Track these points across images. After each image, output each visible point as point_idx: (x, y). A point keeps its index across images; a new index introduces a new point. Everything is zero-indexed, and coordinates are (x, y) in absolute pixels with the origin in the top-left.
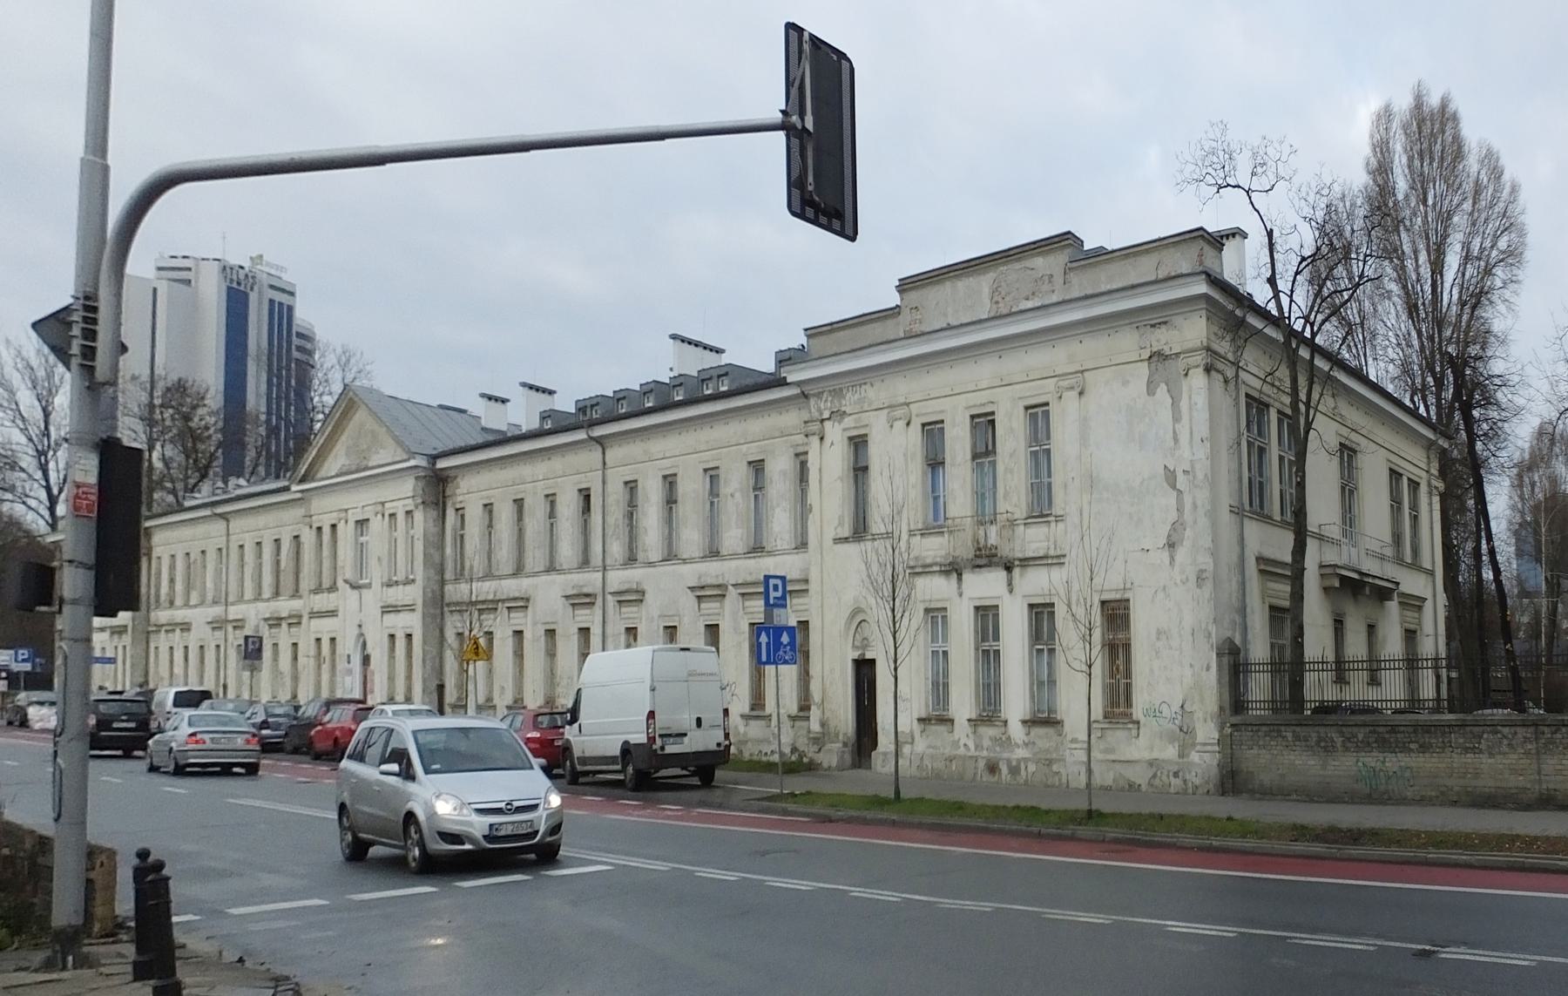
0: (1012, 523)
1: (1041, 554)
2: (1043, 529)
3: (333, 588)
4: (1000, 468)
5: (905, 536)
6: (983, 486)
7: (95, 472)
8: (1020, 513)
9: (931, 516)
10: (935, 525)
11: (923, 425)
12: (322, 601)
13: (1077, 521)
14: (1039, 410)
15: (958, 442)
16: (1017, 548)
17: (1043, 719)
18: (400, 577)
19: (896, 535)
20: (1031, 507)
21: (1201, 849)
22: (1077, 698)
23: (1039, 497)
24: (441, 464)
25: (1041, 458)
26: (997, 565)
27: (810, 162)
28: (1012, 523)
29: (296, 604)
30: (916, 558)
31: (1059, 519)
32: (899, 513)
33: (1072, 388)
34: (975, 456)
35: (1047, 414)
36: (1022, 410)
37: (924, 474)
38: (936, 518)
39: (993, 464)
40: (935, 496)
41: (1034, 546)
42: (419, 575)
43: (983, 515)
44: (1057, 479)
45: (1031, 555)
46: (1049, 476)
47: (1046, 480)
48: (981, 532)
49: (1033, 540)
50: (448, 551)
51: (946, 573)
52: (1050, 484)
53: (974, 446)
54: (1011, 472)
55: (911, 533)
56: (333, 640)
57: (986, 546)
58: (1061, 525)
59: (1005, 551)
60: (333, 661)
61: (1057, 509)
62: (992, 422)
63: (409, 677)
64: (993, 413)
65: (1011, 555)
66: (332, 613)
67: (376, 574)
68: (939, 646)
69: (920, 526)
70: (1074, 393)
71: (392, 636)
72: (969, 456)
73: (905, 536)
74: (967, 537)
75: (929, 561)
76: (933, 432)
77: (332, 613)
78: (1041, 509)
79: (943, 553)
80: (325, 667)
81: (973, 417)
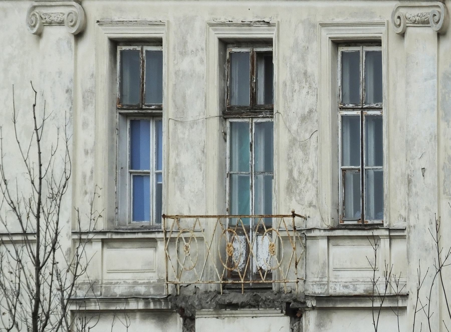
0: (304, 235)
1: (360, 290)
2: (366, 249)
4: (281, 138)
5: (65, 242)
6: (243, 165)
8: (321, 215)
9: (127, 208)
10: (138, 220)
11: (115, 43)
13: (430, 240)
14: (363, 50)
15: (192, 84)
16: (311, 278)
19: (46, 237)
20: (341, 209)
21: (306, 266)
23: (358, 196)
25: (362, 127)
26: (269, 305)
27: (364, 202)
28: (304, 235)
30: (93, 286)
31: (396, 234)
32: (56, 197)
33: (425, 23)
34: (227, 112)
35: (376, 60)
36: (327, 47)
37: (114, 130)
38: (138, 211)
39: (267, 130)
40: (137, 173)
41: (346, 276)
43: (244, 215)
44: (394, 169)
45: (340, 290)
46: (379, 160)
47: (371, 167)
48: (239, 246)
49: (345, 265)
51: (160, 315)
52: (379, 176)
53: (226, 94)
54: (304, 147)
55: (81, 238)
57: (247, 272)
58: (399, 247)
59: (288, 280)
61: (393, 216)
62: (267, 59)
64: (268, 42)
65: (300, 289)
69: (101, 225)
70: (429, 32)
72: (214, 108)
73: (65, 242)
74: (211, 249)
75: (119, 291)
76: (136, 64)
78: (362, 209)
79: (153, 277)
81: (224, 43)
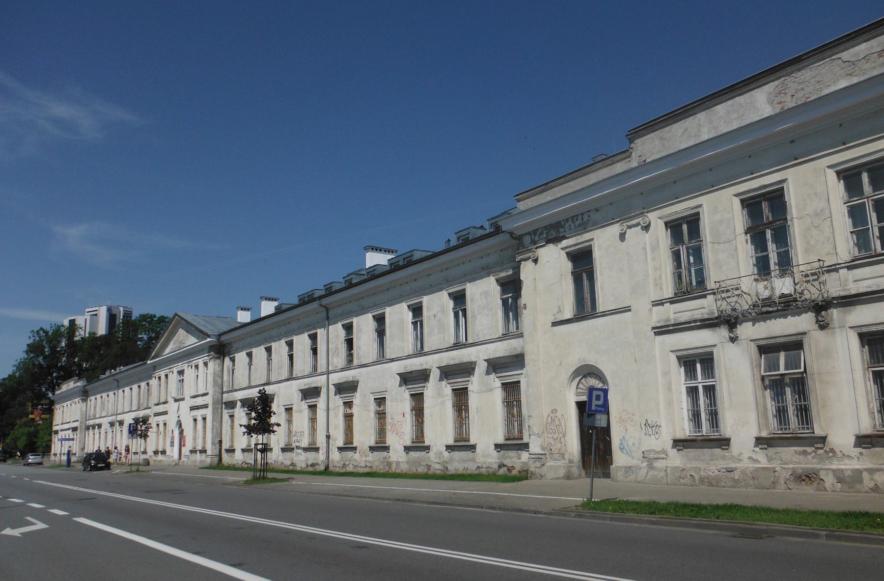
3: (165, 403)
7: (397, 307)
12: (161, 408)
17: (418, 445)
18: (162, 400)
22: (744, 413)
24: (223, 338)
29: (147, 412)
42: (211, 391)
50: (225, 378)
56: (165, 424)
60: (165, 433)
63: (204, 438)
66: (165, 413)
67: (187, 393)
68: (349, 411)
71: (195, 420)
77: (165, 413)
80: (161, 437)
